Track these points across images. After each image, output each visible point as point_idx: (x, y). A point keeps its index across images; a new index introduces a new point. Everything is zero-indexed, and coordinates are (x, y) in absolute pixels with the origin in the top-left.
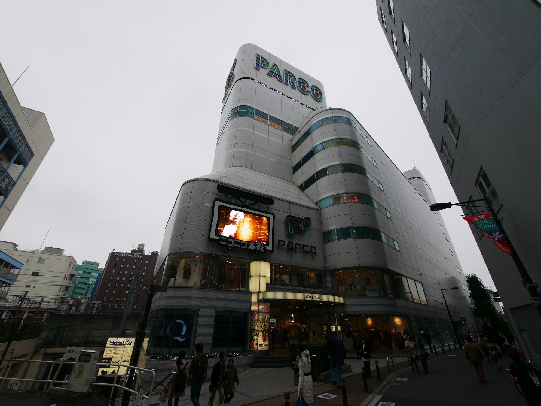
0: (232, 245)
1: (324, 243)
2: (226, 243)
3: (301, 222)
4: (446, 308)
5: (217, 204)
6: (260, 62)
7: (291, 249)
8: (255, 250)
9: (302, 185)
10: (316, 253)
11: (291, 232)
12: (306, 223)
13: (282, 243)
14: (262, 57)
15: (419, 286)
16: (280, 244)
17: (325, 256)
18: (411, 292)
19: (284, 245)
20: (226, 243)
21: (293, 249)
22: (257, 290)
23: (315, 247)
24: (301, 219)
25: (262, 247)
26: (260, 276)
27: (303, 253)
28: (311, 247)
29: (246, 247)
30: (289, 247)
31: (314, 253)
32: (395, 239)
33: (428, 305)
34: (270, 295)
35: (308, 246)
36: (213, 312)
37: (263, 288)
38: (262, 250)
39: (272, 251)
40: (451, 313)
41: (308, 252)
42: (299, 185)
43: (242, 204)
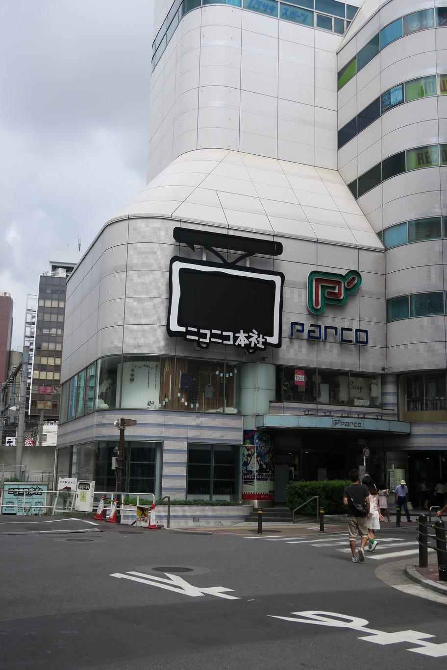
0: (207, 340)
3: (339, 283)
9: (355, 182)
10: (366, 342)
11: (317, 304)
12: (349, 284)
13: (299, 327)
19: (302, 331)
23: (366, 332)
25: (261, 340)
29: (231, 342)
30: (312, 334)
35: (351, 330)
36: (184, 446)
38: (260, 346)
41: (351, 341)
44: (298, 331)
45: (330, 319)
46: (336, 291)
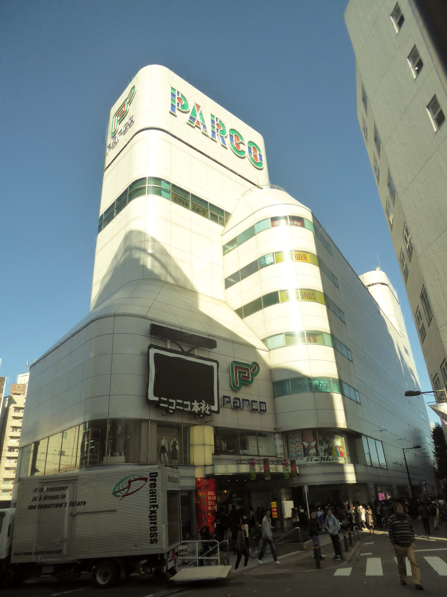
0: (174, 408)
1: (274, 397)
2: (182, 408)
4: (406, 470)
5: (153, 352)
6: (177, 101)
7: (237, 407)
8: (200, 412)
10: (265, 411)
12: (253, 371)
13: (228, 400)
14: (178, 92)
15: (379, 444)
16: (225, 402)
17: (276, 415)
18: (369, 453)
20: (182, 408)
21: (240, 407)
22: (202, 463)
23: (264, 403)
24: (248, 365)
26: (204, 445)
27: (250, 411)
28: (260, 402)
29: (189, 409)
30: (236, 405)
31: (263, 411)
32: (356, 388)
33: (387, 469)
34: (222, 469)
35: (256, 402)
37: (209, 459)
38: (207, 412)
39: (218, 412)
40: (411, 476)
41: (257, 410)
42: (237, 308)
43: (180, 350)
44: (227, 402)
45: (244, 393)
46: (247, 375)
